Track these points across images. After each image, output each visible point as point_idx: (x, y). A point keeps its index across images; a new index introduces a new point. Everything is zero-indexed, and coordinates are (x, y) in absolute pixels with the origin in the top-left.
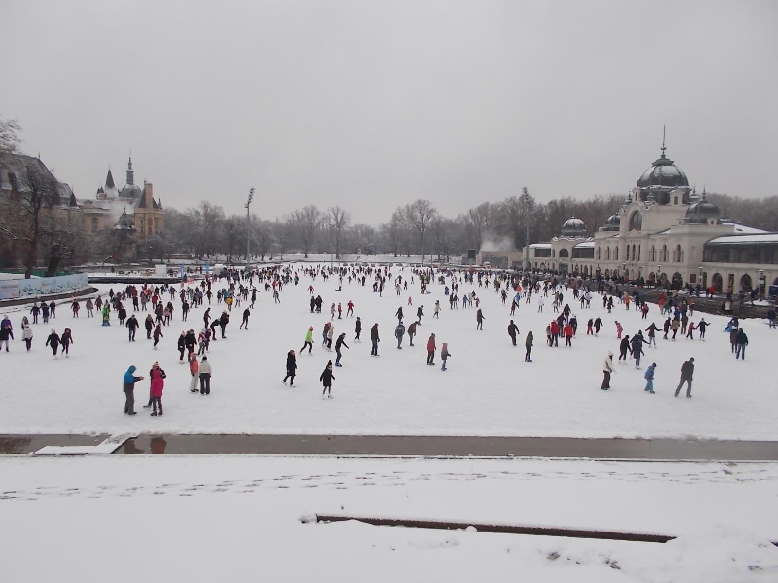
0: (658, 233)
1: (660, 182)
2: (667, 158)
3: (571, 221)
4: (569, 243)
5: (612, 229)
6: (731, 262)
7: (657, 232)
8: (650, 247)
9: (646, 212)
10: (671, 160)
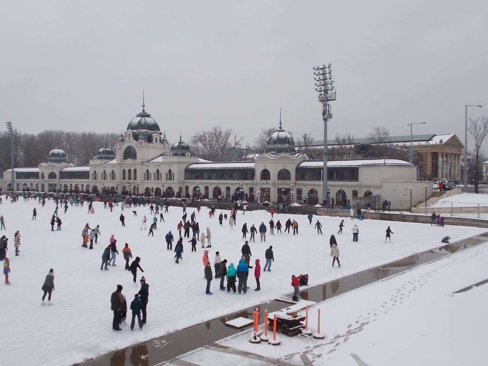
0: (147, 161)
1: (146, 128)
2: (146, 112)
3: (56, 151)
4: (57, 168)
5: (104, 158)
6: (205, 179)
7: (146, 161)
8: (145, 171)
9: (140, 147)
10: (149, 114)
